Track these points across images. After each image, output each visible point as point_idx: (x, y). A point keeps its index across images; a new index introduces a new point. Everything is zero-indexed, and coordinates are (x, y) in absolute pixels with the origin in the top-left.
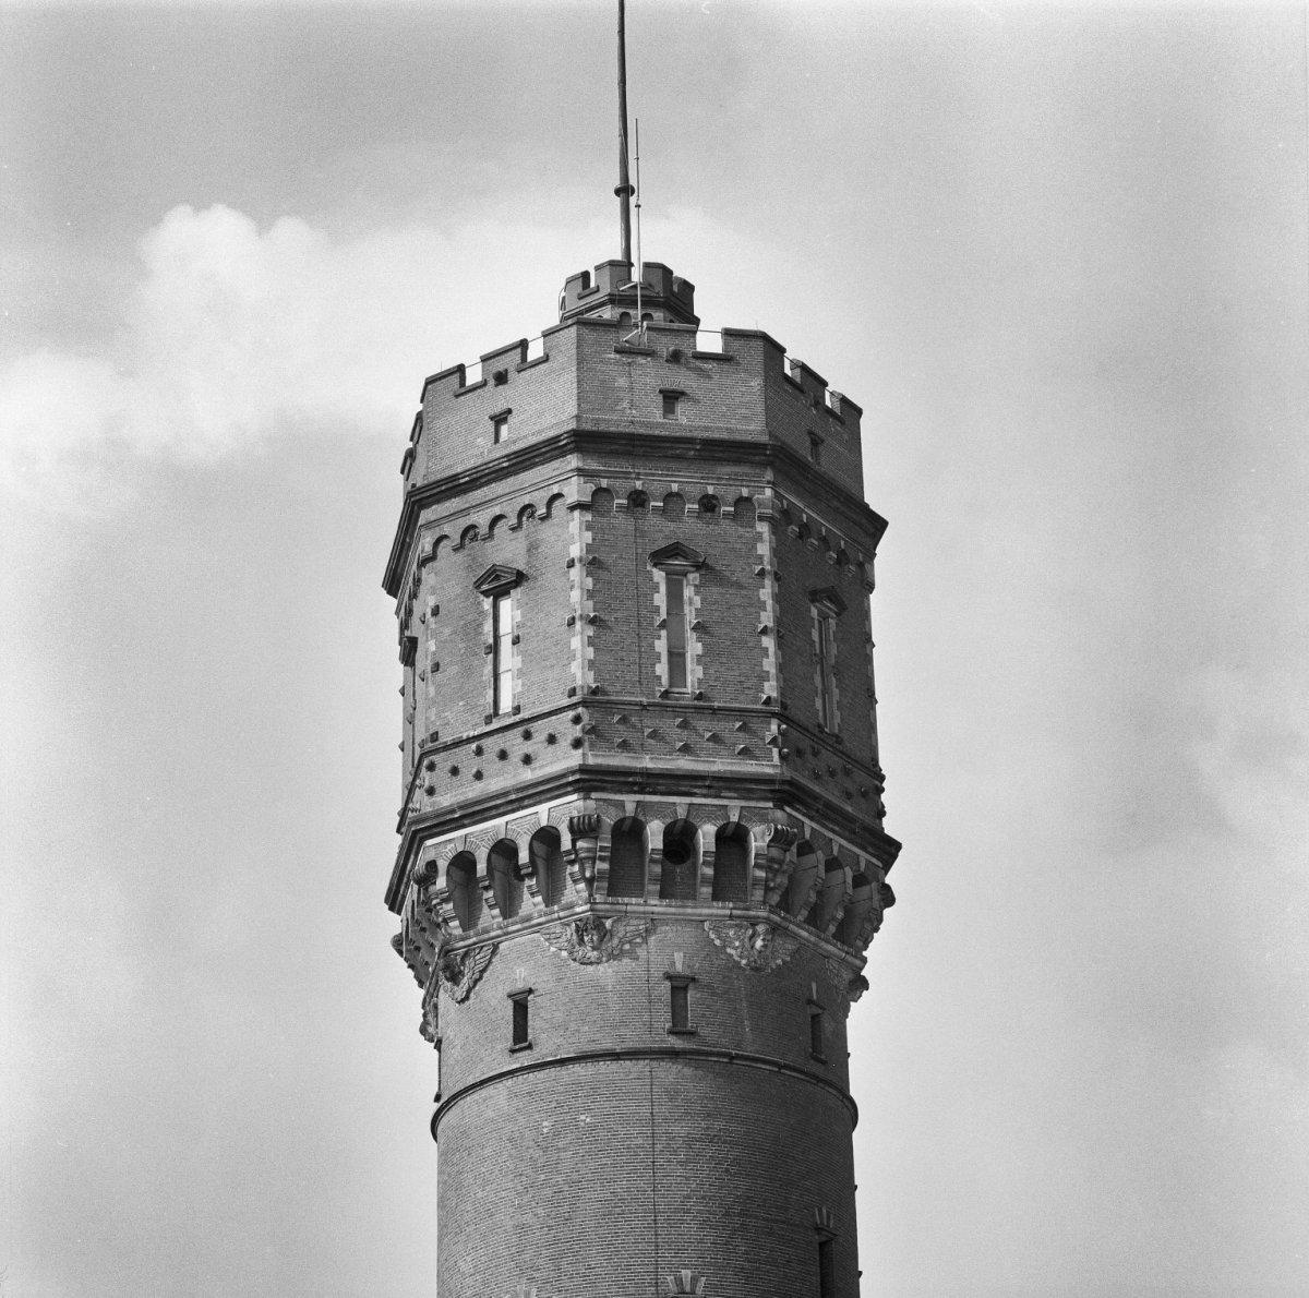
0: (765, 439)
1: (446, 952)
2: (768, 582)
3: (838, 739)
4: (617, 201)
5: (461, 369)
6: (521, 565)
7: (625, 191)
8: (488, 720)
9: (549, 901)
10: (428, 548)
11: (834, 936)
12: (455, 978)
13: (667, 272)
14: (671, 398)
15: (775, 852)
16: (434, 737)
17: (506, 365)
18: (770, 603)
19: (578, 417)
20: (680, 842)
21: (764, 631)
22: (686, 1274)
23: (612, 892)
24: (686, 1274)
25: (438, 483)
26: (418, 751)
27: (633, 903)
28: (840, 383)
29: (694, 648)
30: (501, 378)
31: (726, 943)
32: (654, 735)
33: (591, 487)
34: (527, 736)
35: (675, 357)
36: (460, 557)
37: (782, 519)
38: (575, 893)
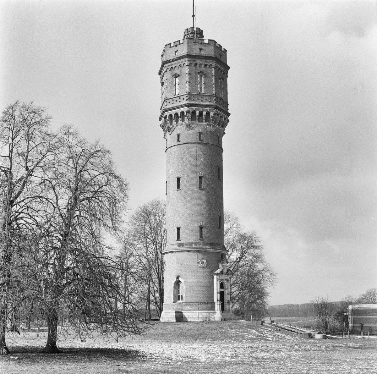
1: (168, 128)
7: (193, 16)
9: (183, 121)
10: (166, 70)
14: (201, 49)
15: (214, 116)
16: (167, 98)
17: (177, 44)
19: (188, 52)
21: (213, 84)
24: (201, 173)
27: (194, 122)
33: (189, 63)
34: (180, 98)
35: (201, 44)
37: (216, 68)
38: (186, 121)
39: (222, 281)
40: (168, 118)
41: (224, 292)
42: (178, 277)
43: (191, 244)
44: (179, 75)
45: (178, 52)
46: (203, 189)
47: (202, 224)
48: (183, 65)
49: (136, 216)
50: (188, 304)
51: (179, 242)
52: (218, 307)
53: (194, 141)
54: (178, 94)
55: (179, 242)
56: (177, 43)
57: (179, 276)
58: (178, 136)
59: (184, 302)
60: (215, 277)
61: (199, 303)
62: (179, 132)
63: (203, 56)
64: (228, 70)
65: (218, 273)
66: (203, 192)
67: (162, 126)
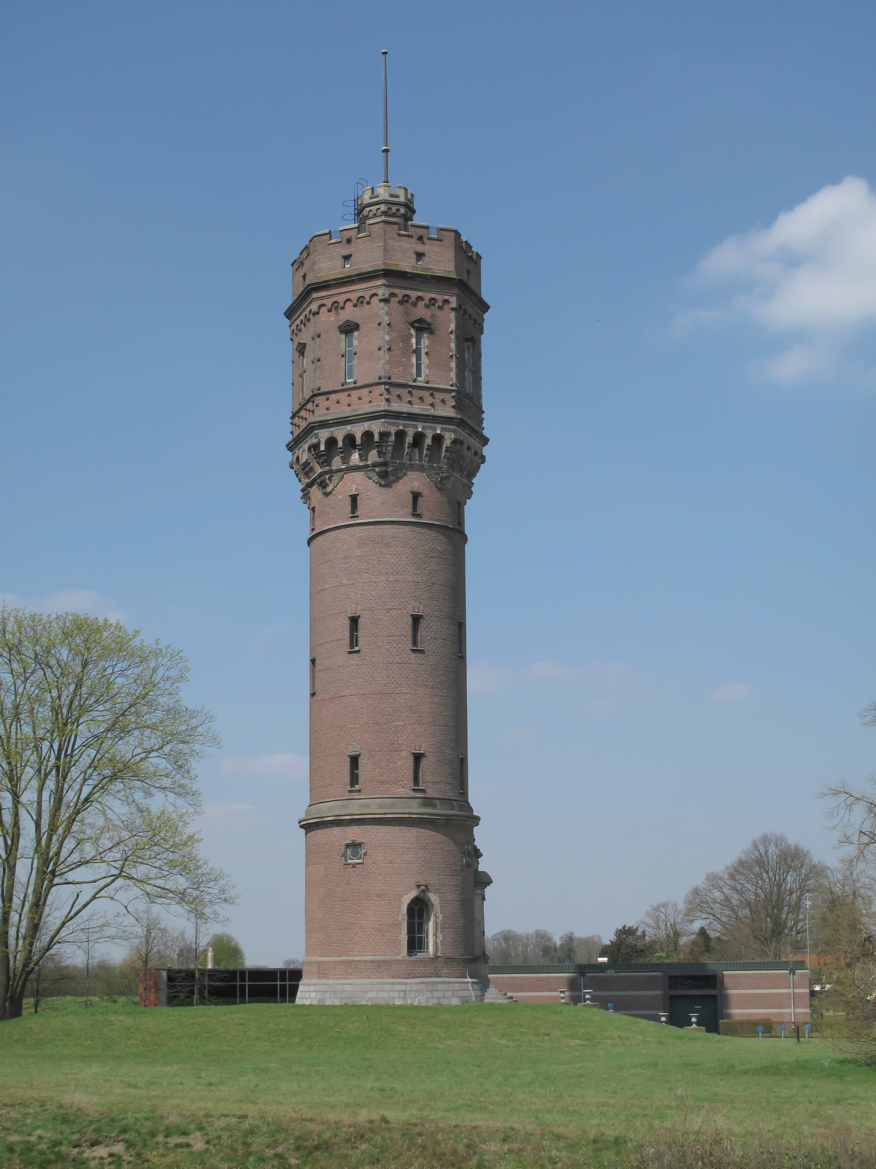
0: (454, 277)
3: (472, 398)
8: (343, 385)
11: (466, 475)
14: (420, 256)
16: (319, 389)
20: (419, 439)
29: (425, 360)
49: (627, 928)
54: (355, 383)
64: (485, 312)
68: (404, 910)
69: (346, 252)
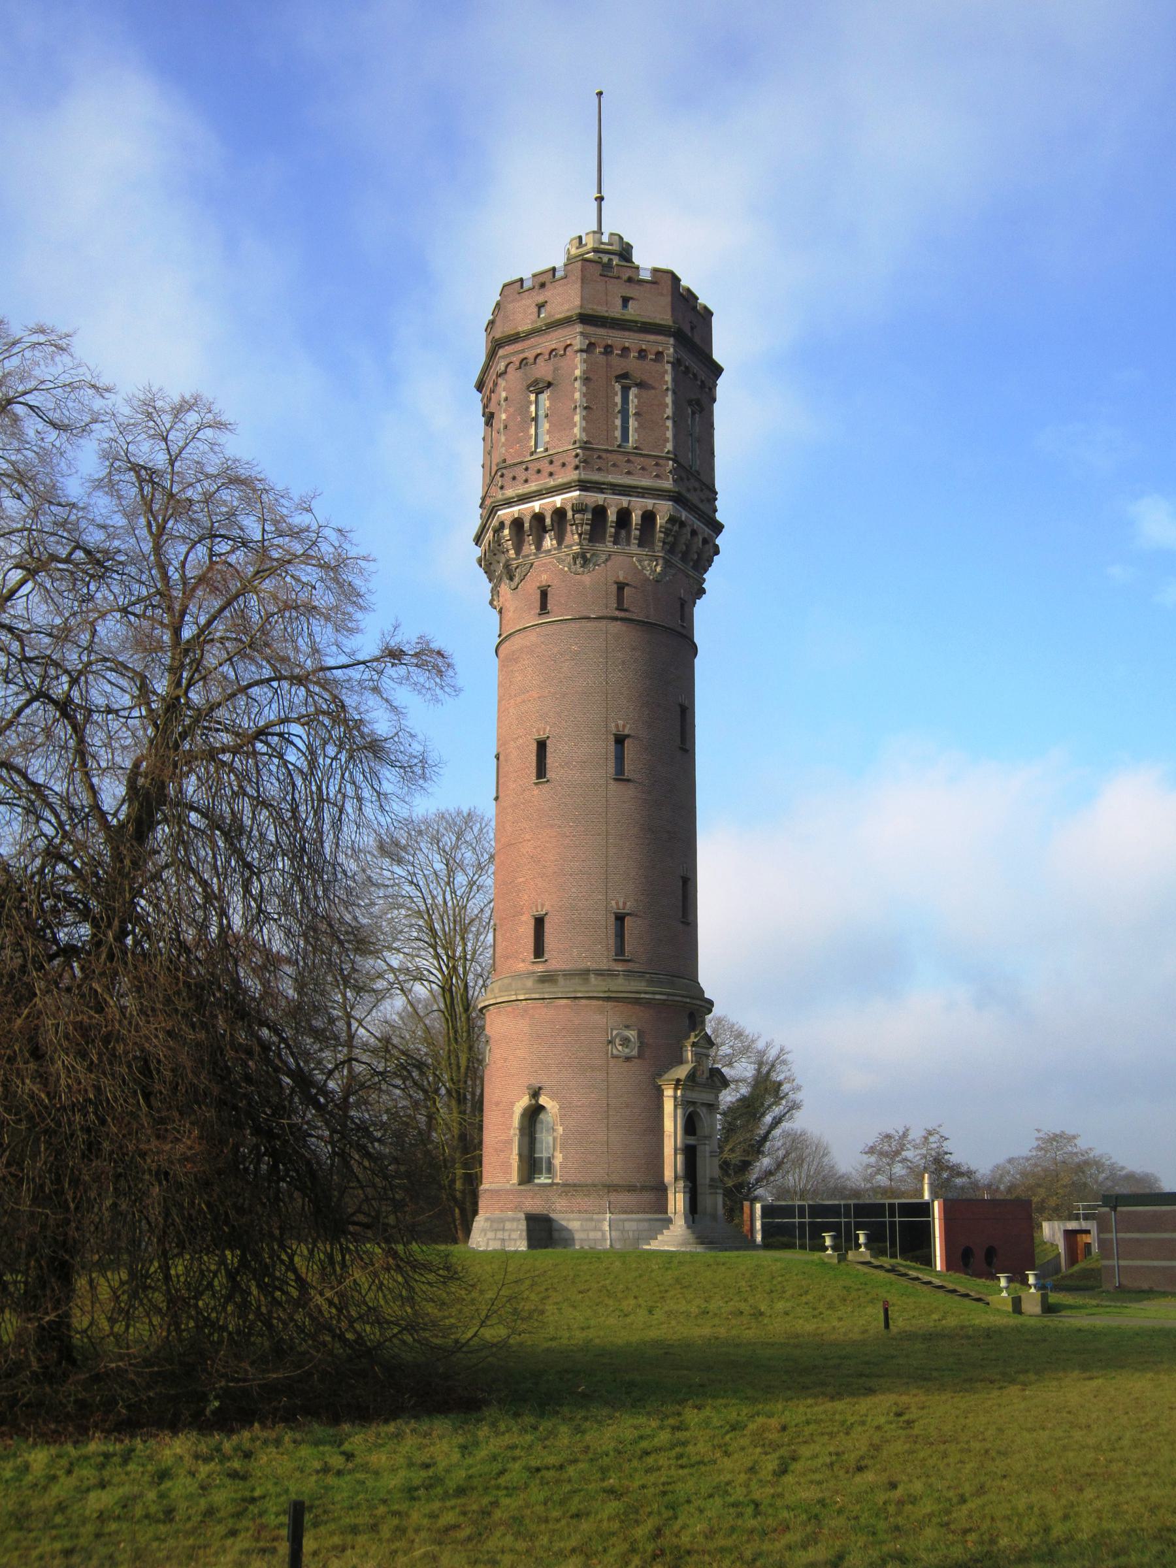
0: (671, 323)
1: (507, 566)
2: (670, 393)
4: (595, 204)
5: (521, 280)
6: (550, 379)
7: (600, 199)
8: (532, 454)
9: (560, 542)
10: (503, 368)
12: (511, 579)
13: (621, 238)
14: (626, 301)
15: (669, 526)
16: (504, 461)
17: (546, 279)
18: (670, 405)
19: (581, 307)
21: (668, 418)
22: (621, 722)
23: (590, 540)
24: (621, 722)
25: (509, 336)
26: (494, 469)
27: (600, 547)
28: (703, 299)
30: (543, 285)
31: (644, 568)
32: (614, 465)
33: (587, 342)
34: (551, 462)
35: (630, 280)
36: (519, 373)
37: (677, 364)
38: (572, 537)
39: (691, 1109)
40: (506, 532)
41: (699, 1148)
42: (535, 1094)
43: (584, 974)
44: (549, 385)
45: (548, 307)
46: (628, 780)
47: (625, 904)
48: (565, 350)
50: (570, 1188)
51: (540, 968)
52: (677, 1201)
53: (604, 613)
55: (540, 968)
56: (545, 276)
57: (540, 1088)
58: (544, 595)
59: (557, 1180)
60: (668, 1092)
61: (611, 1188)
62: (544, 578)
63: (636, 322)
65: (678, 1080)
66: (629, 791)
67: (486, 563)
68: (516, 1121)
69: (541, 299)
